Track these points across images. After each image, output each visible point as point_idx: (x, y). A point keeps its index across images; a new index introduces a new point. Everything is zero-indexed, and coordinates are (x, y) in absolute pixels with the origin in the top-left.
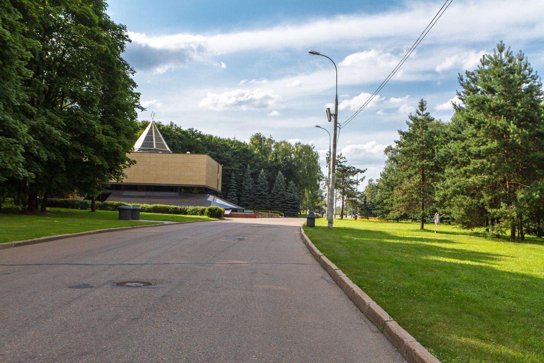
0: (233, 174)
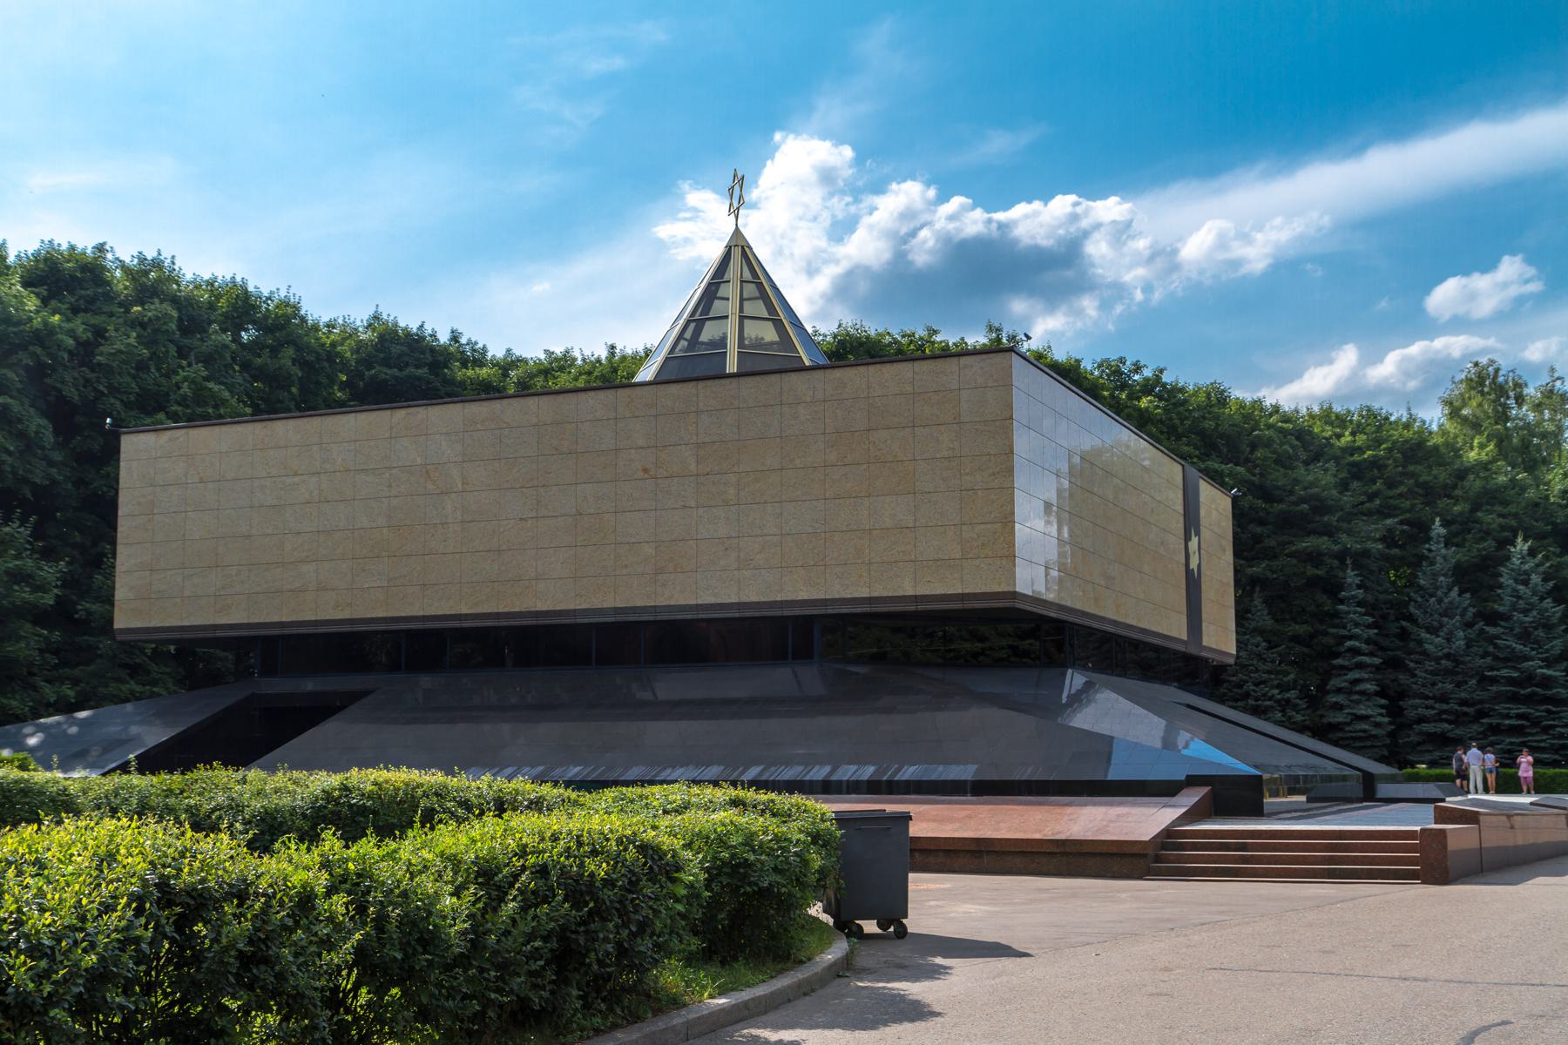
0: (1351, 577)
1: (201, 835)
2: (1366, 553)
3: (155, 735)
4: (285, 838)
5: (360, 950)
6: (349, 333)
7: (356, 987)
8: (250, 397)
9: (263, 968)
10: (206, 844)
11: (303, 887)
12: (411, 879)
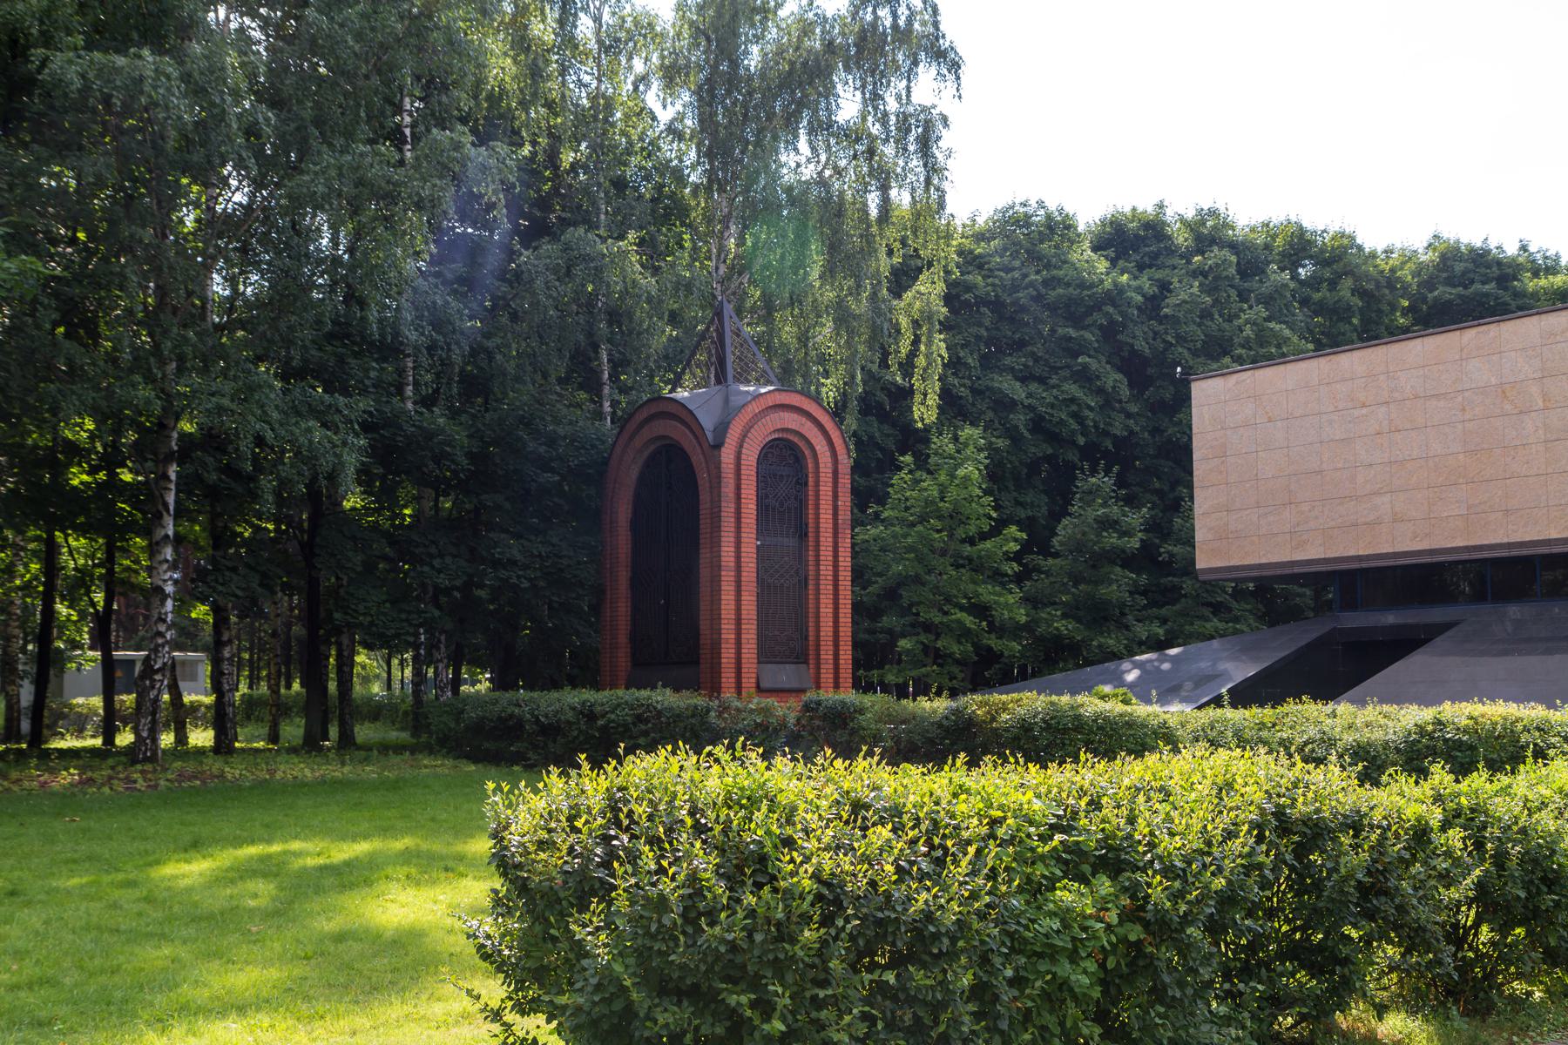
1: (1311, 766)
3: (1242, 671)
4: (1391, 770)
5: (1480, 885)
6: (1409, 257)
7: (1477, 925)
8: (1311, 332)
9: (1383, 899)
10: (1317, 775)
11: (1418, 820)
12: (1530, 815)
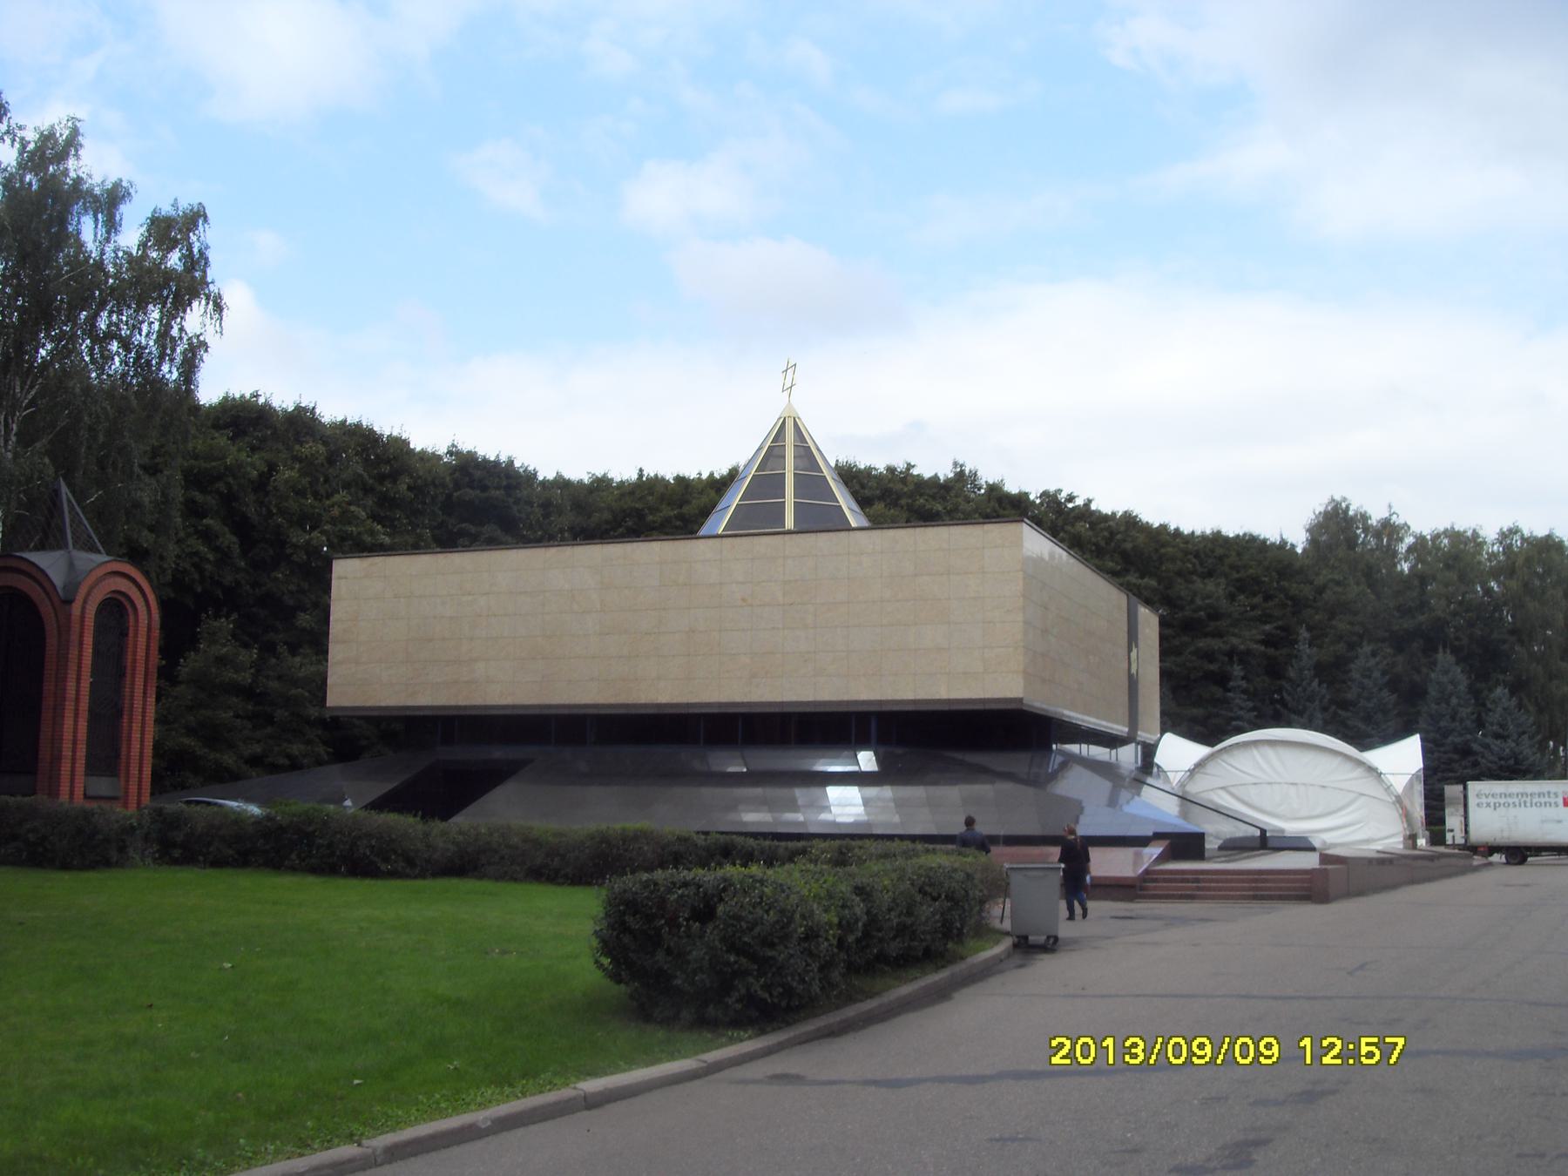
0: (1237, 670)
2: (1248, 652)
